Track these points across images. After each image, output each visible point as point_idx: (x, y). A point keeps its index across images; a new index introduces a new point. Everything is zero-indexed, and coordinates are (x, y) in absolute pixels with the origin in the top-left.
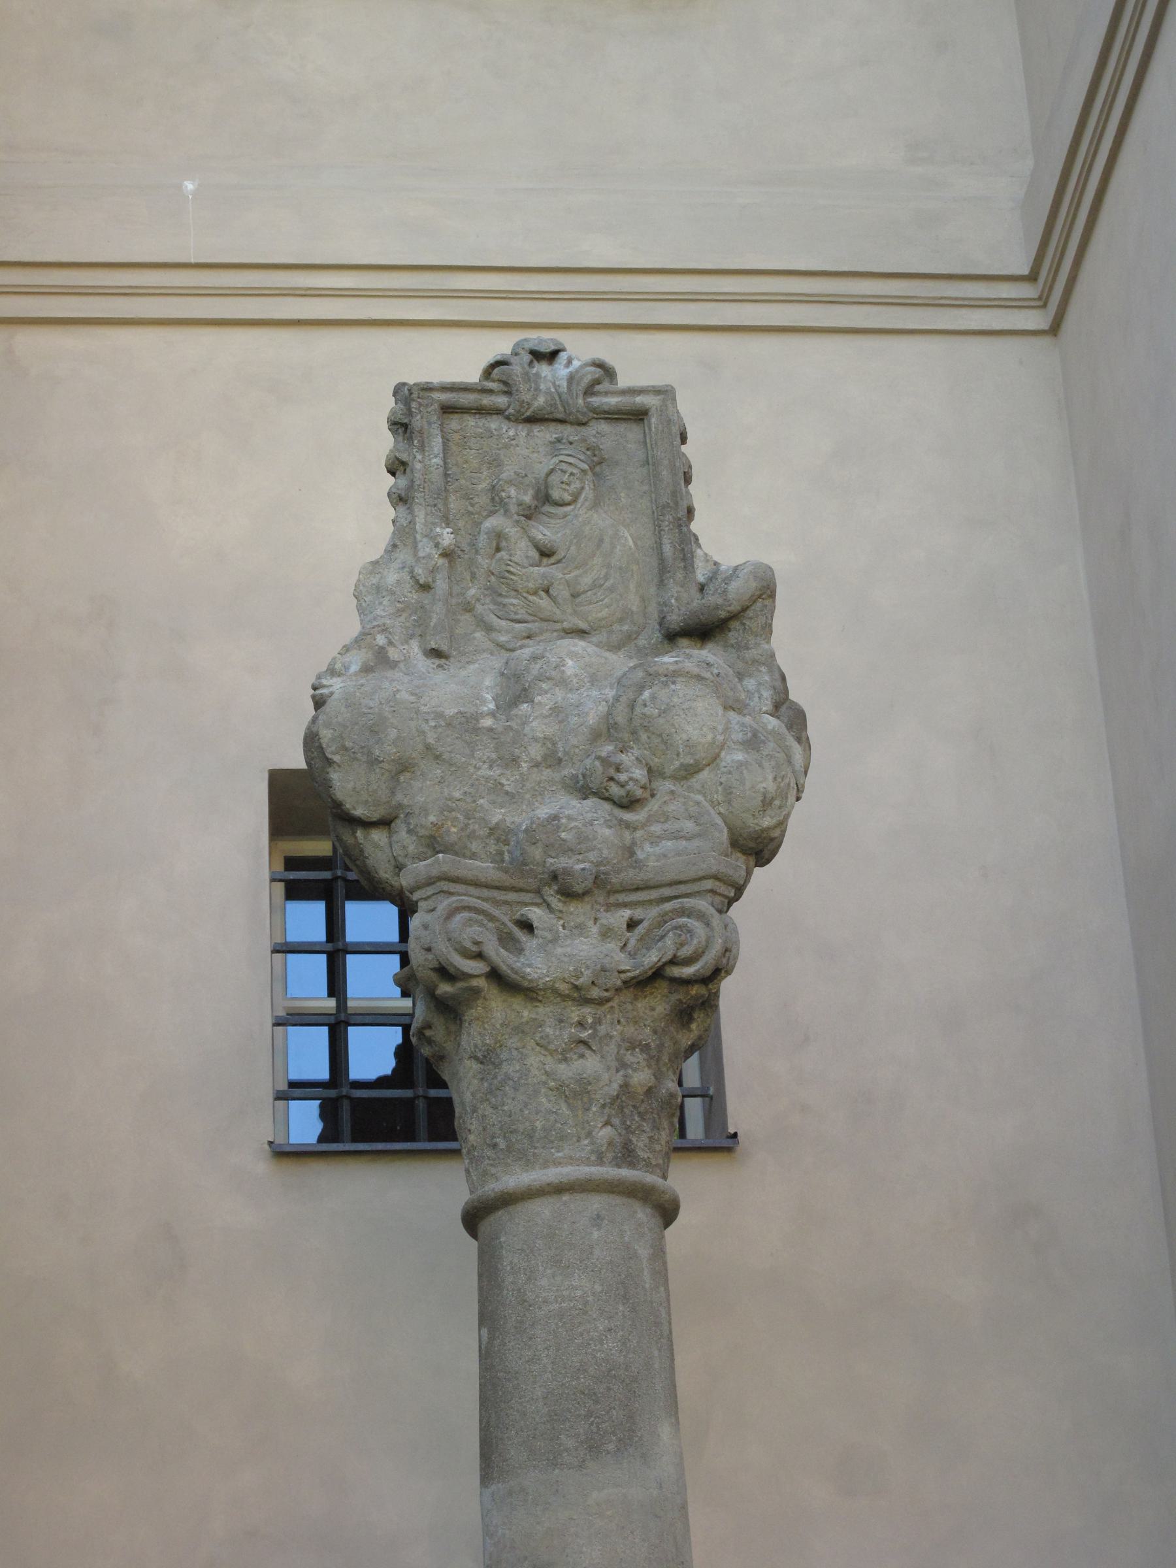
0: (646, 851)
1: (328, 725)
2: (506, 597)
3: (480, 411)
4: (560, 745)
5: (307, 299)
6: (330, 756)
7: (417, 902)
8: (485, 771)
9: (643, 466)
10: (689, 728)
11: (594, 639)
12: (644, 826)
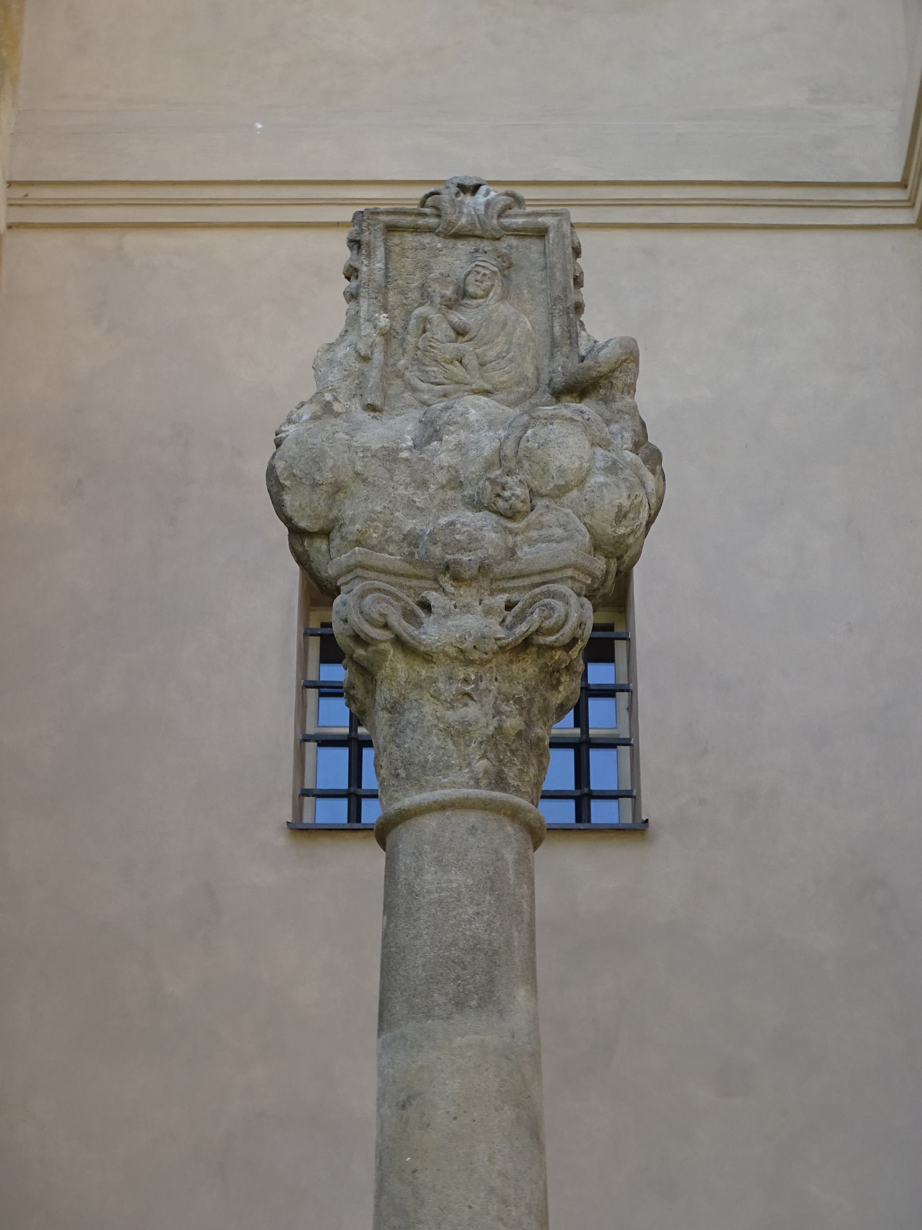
0: (524, 553)
1: (281, 458)
2: (429, 366)
3: (416, 230)
4: (461, 472)
6: (282, 481)
8: (401, 491)
10: (561, 457)
11: (496, 397)
12: (524, 531)
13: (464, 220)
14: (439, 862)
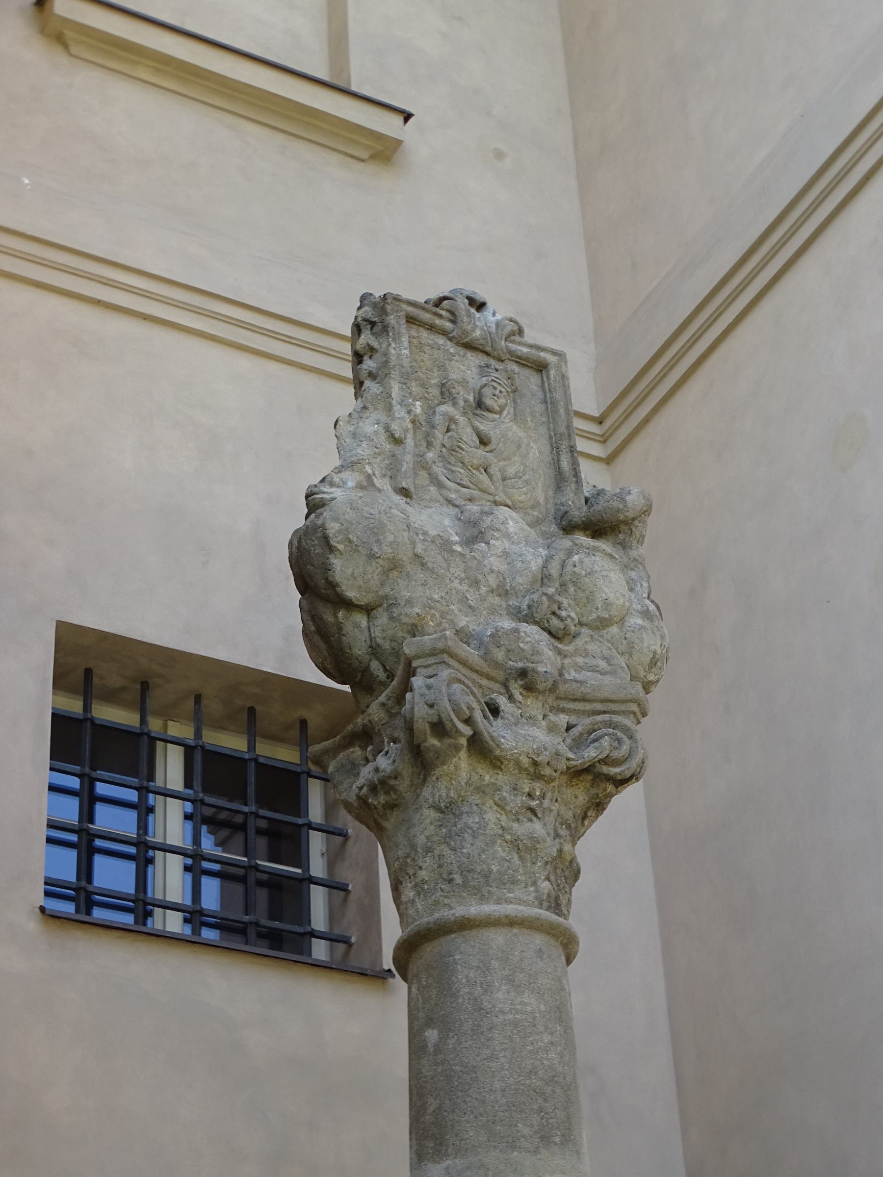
5: (107, 288)
6: (333, 543)
7: (416, 668)
9: (541, 403)
12: (572, 656)
13: (478, 333)
14: (510, 980)
